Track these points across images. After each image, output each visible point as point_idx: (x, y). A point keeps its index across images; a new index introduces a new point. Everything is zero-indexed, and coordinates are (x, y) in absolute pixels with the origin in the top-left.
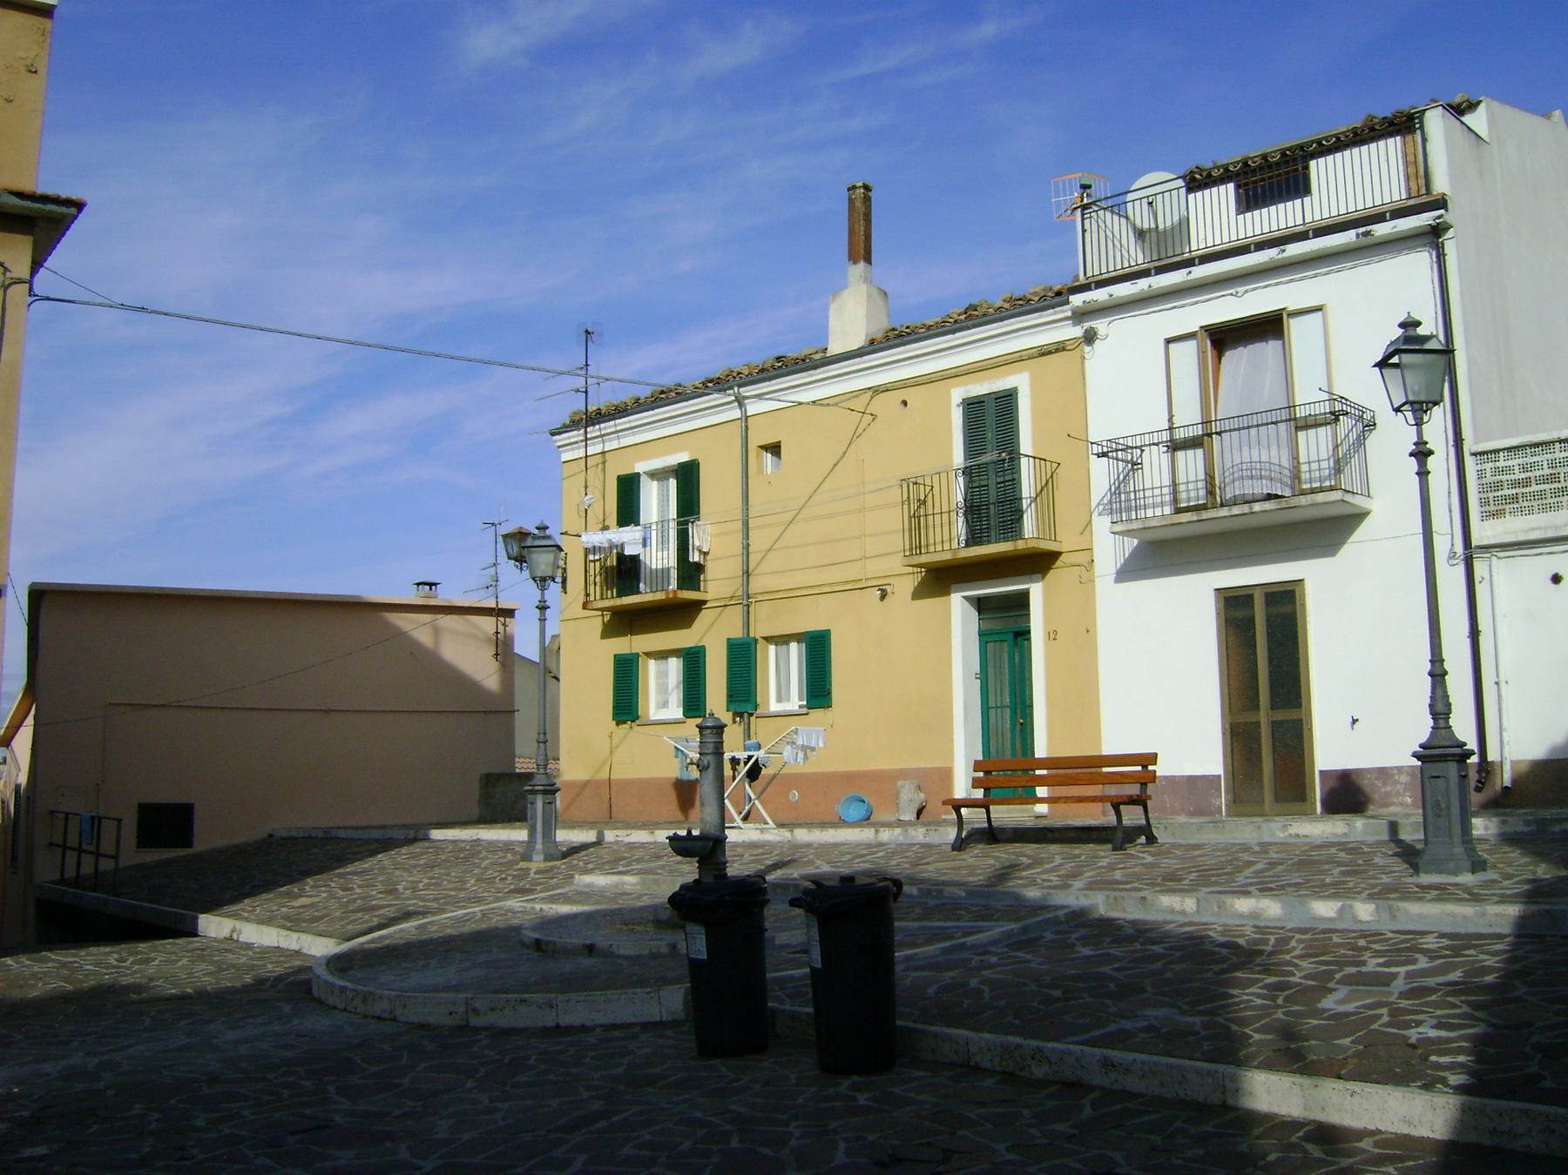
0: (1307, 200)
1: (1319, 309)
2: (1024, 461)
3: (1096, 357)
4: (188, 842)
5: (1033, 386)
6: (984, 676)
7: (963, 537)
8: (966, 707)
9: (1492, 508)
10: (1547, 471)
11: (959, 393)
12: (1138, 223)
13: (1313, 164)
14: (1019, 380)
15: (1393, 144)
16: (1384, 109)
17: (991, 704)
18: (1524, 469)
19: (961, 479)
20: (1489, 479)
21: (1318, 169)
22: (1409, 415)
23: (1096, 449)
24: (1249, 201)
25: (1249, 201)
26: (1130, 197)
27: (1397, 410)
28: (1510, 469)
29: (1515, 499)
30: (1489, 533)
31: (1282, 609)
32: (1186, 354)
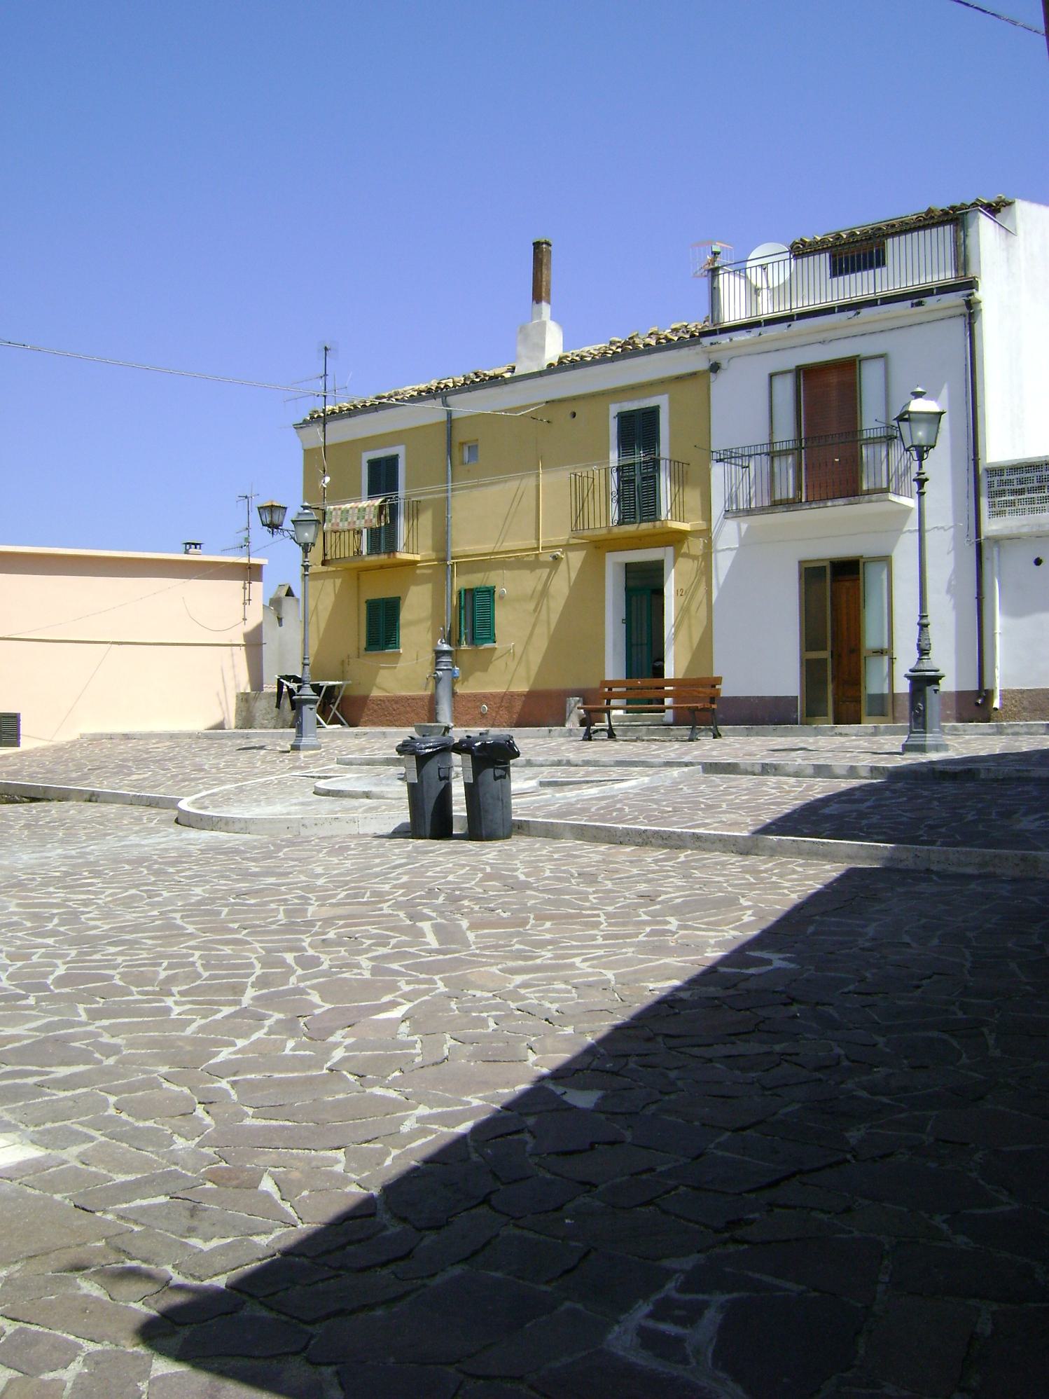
0: (884, 269)
1: (881, 356)
2: (511, 690)
3: (718, 385)
4: (18, 745)
5: (671, 402)
6: (628, 621)
7: (616, 517)
8: (615, 645)
9: (997, 509)
10: (1036, 484)
11: (614, 409)
12: (754, 282)
13: (890, 241)
14: (661, 401)
15: (948, 229)
16: (941, 203)
17: (634, 641)
18: (1021, 482)
19: (615, 475)
20: (996, 488)
21: (891, 245)
22: (914, 453)
23: (715, 456)
24: (838, 269)
25: (838, 269)
26: (749, 264)
27: (907, 450)
28: (1010, 482)
29: (1012, 503)
30: (994, 528)
31: (657, 664)
32: (785, 388)
